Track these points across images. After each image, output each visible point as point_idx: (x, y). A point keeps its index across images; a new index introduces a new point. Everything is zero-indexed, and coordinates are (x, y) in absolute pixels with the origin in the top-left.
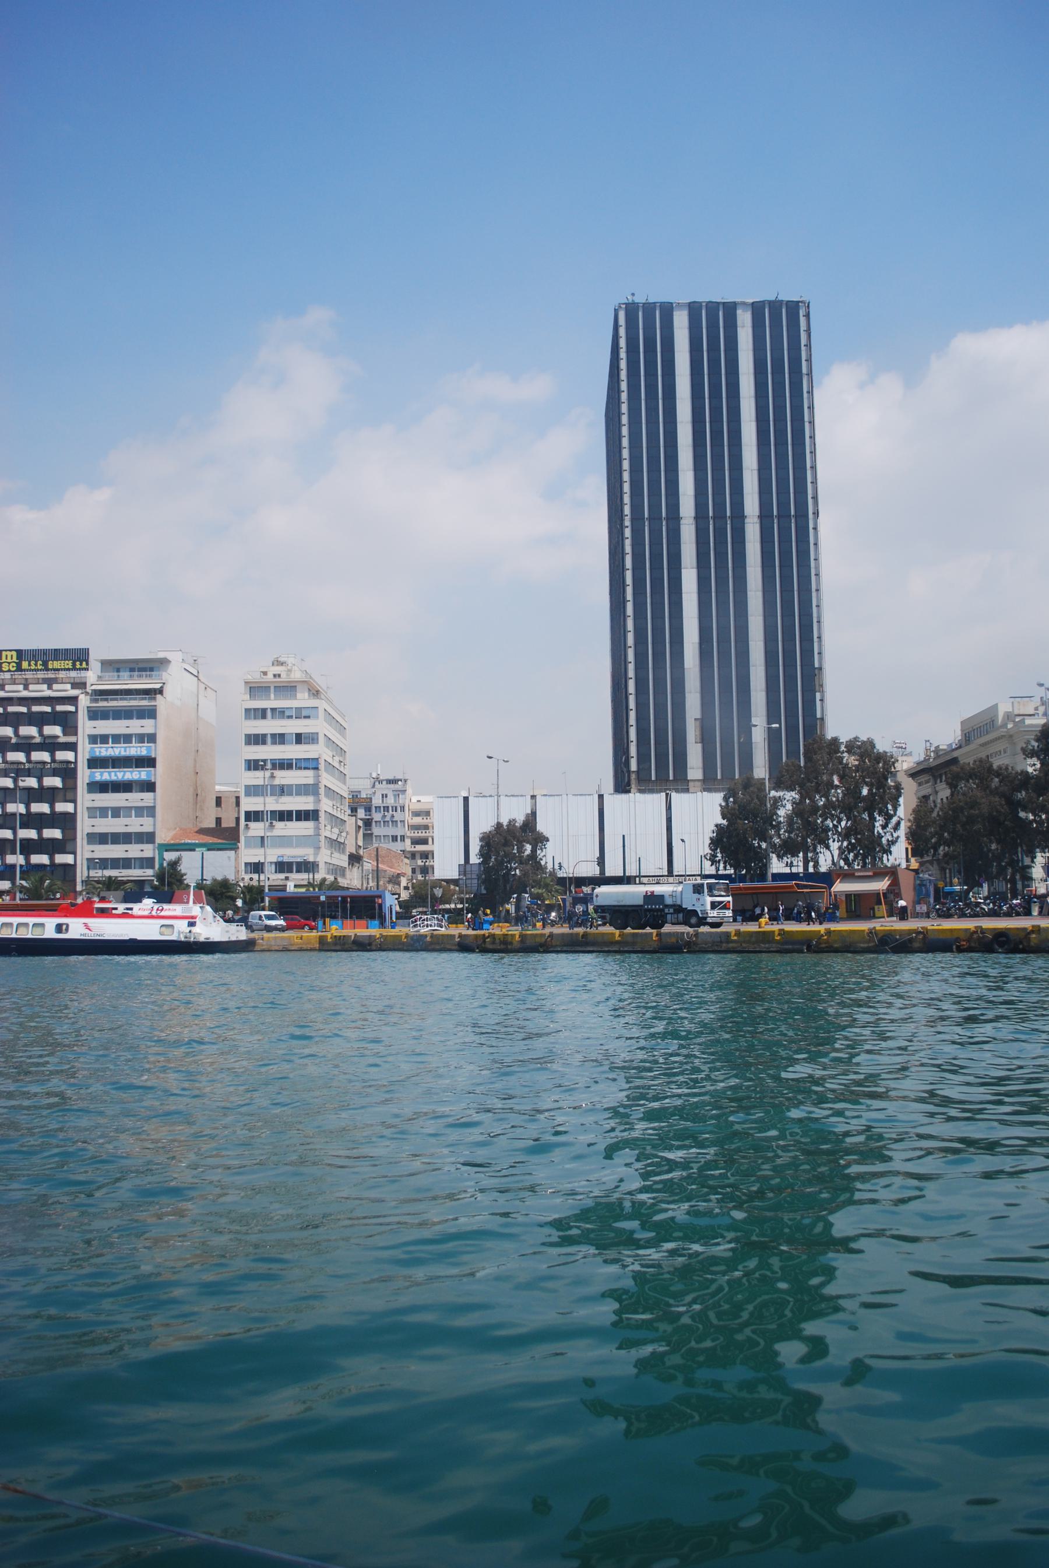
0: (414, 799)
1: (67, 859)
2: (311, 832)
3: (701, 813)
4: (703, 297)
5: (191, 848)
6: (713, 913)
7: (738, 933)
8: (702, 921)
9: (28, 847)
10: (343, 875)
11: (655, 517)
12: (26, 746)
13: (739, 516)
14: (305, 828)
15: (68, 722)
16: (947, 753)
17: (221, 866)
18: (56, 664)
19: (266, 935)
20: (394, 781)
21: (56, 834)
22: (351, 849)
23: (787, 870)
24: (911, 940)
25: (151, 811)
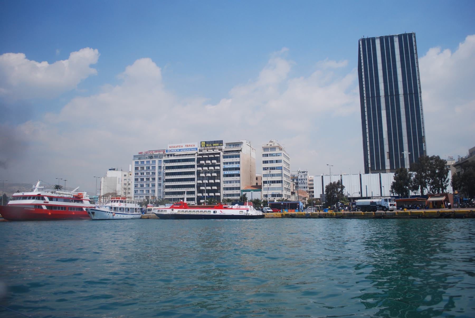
0: (309, 177)
1: (219, 194)
2: (281, 186)
3: (389, 178)
4: (383, 35)
5: (249, 191)
6: (391, 207)
7: (398, 213)
8: (387, 209)
9: (208, 191)
10: (290, 198)
11: (373, 96)
12: (208, 166)
13: (397, 94)
14: (279, 185)
15: (218, 159)
16: (465, 159)
17: (257, 195)
18: (215, 145)
19: (267, 214)
20: (304, 172)
21: (216, 188)
22: (292, 190)
23: (414, 195)
24: (450, 215)
25: (239, 181)
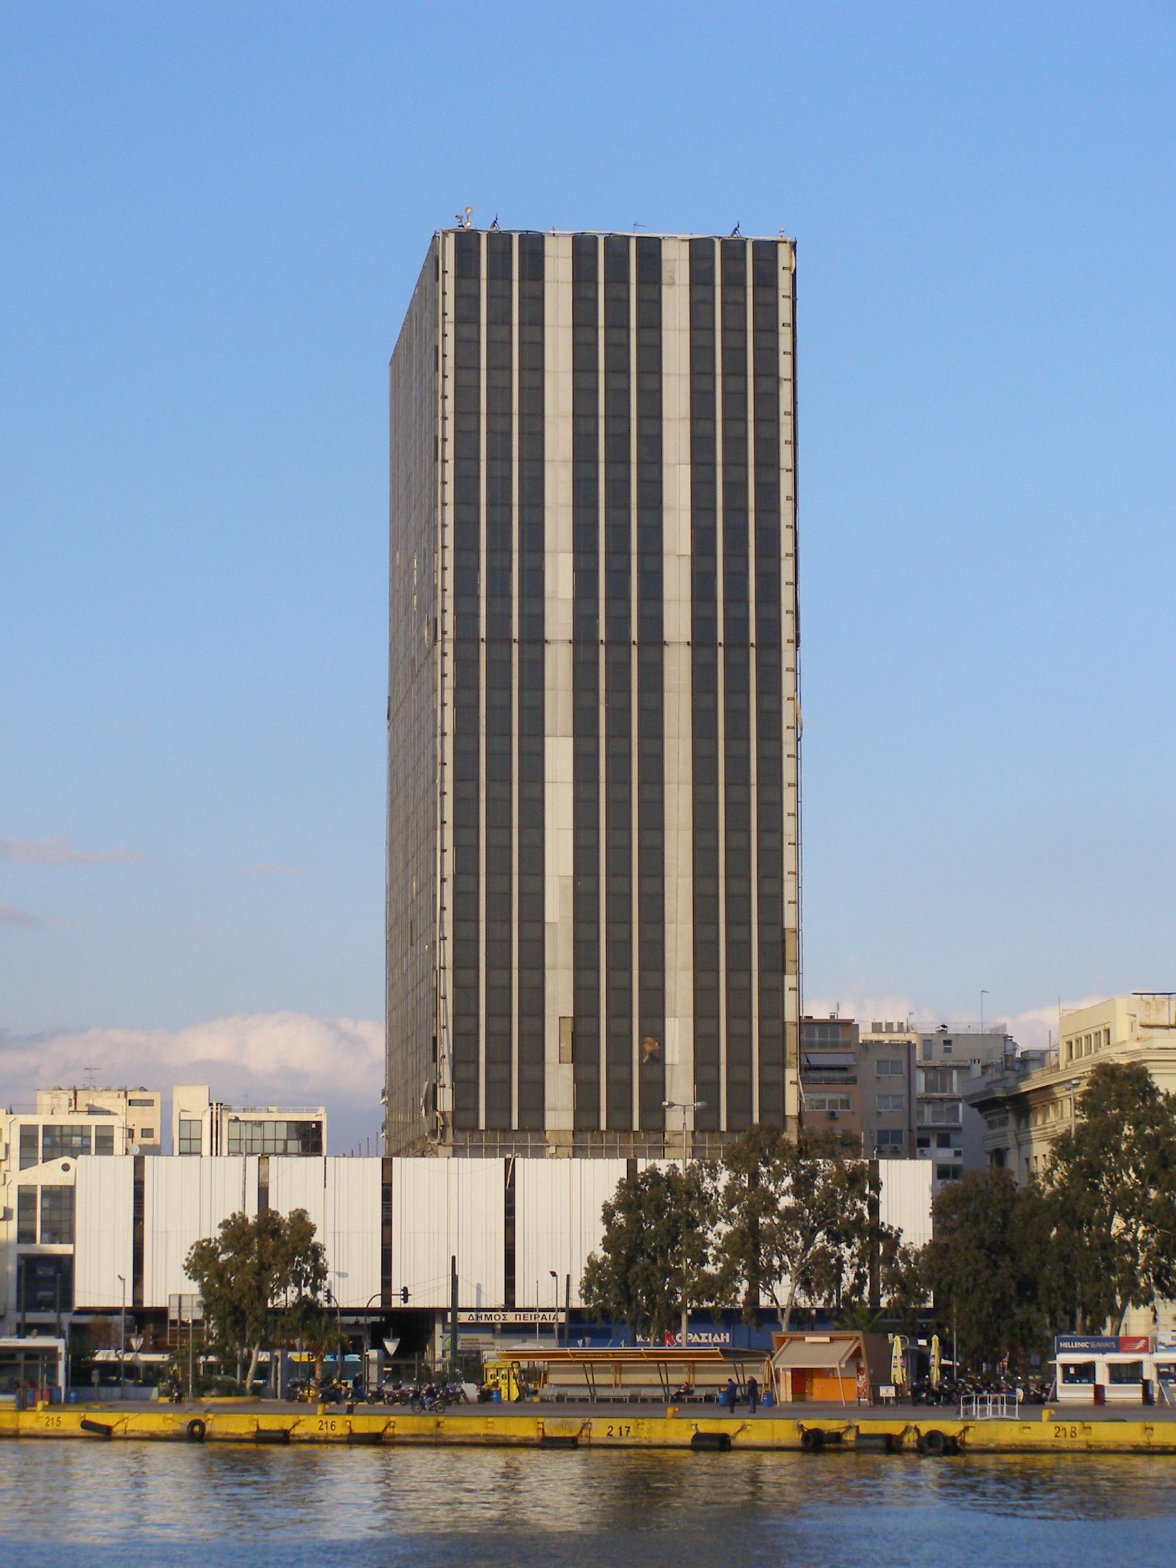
3: (568, 1207)
